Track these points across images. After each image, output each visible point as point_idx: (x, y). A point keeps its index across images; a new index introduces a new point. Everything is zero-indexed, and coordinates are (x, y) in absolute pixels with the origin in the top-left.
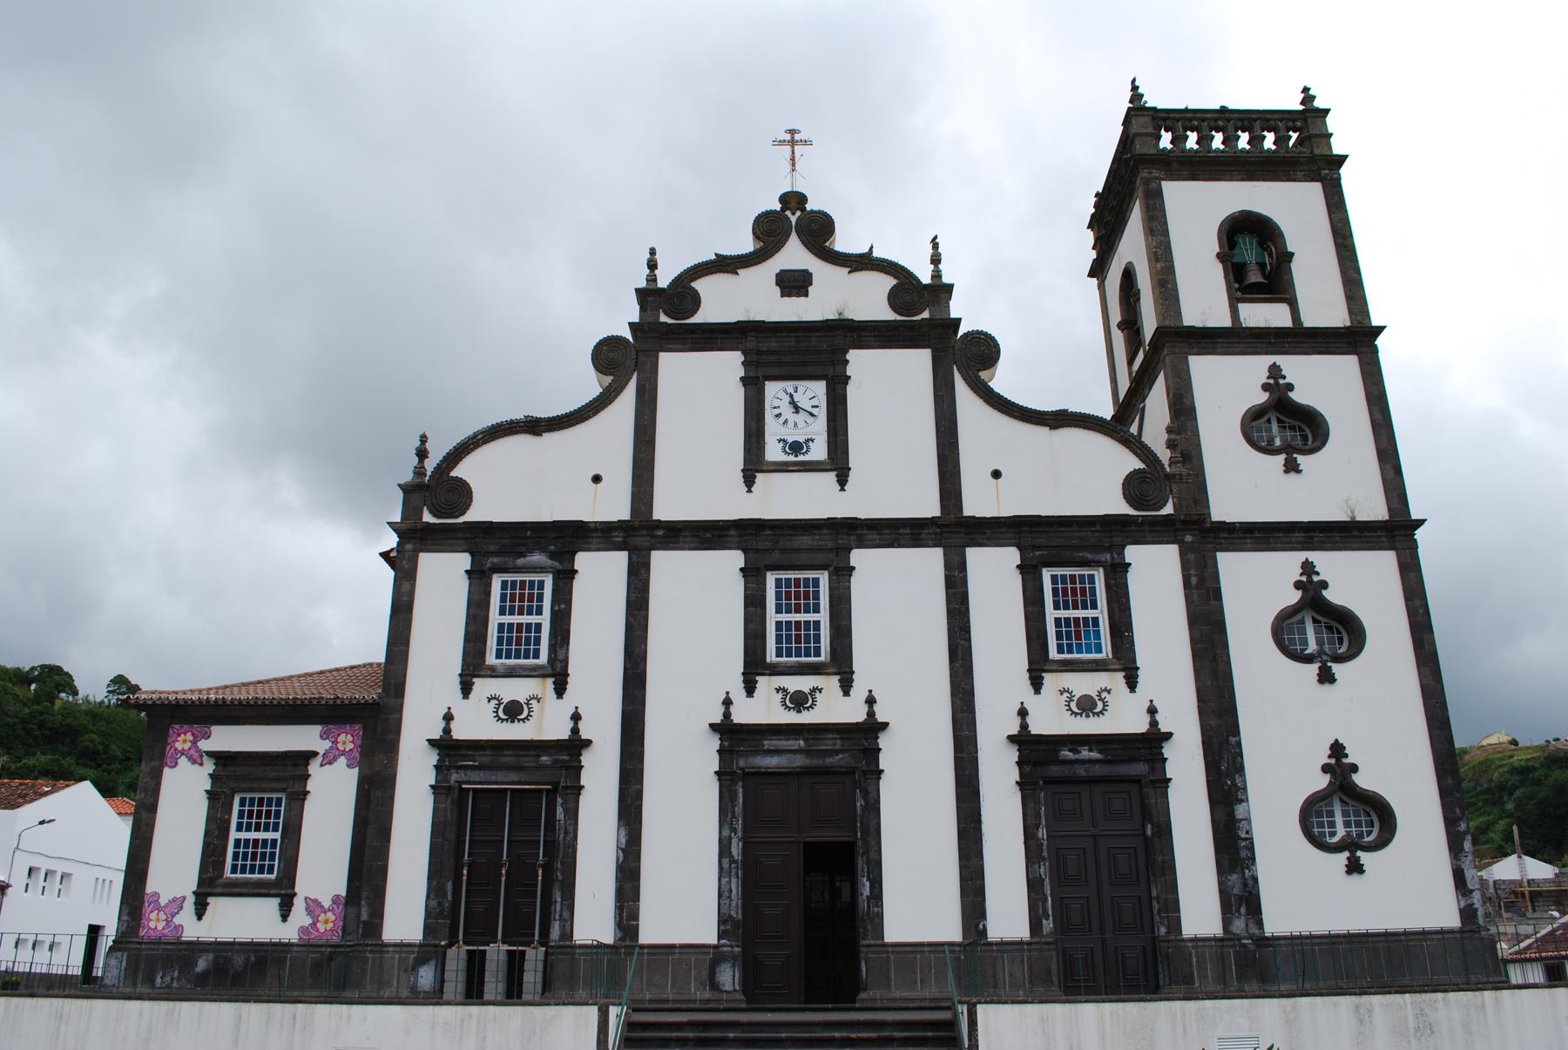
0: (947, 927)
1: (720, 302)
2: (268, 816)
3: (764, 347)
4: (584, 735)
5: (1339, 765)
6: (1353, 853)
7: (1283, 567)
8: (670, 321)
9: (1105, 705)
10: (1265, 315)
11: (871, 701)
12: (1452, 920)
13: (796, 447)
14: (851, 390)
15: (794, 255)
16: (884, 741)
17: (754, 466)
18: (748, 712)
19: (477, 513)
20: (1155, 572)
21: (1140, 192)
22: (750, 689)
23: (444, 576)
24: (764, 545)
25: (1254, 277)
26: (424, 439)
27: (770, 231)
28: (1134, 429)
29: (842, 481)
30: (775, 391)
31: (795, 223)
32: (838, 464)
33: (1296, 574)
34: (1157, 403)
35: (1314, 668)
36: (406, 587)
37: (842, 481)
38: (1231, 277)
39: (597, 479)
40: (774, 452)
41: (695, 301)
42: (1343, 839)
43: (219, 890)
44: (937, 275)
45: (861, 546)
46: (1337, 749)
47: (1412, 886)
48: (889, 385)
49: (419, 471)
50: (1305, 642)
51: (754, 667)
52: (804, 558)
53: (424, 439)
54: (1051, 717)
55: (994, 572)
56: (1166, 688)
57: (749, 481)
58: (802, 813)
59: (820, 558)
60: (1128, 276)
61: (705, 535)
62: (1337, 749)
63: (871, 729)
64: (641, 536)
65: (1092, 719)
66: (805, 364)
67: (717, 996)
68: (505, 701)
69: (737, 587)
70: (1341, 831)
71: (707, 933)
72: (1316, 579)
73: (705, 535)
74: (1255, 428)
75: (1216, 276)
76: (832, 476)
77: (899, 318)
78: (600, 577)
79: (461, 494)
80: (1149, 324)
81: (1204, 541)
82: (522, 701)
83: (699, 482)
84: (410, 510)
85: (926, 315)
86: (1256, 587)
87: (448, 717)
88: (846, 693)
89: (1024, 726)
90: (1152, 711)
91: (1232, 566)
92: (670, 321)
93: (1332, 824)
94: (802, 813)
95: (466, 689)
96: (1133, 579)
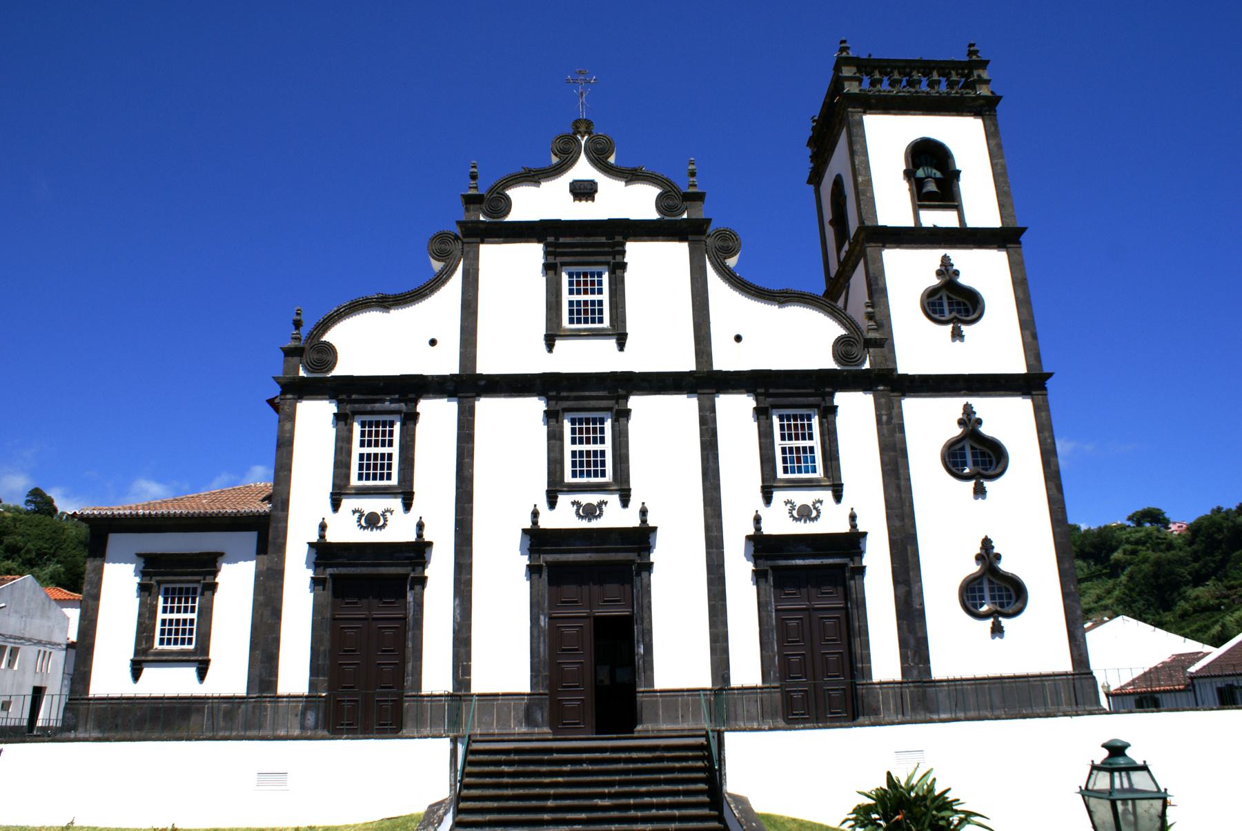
5: (987, 555)
10: (935, 218)
11: (644, 512)
22: (552, 504)
24: (563, 394)
29: (621, 346)
33: (959, 414)
36: (288, 426)
37: (621, 346)
41: (507, 204)
46: (987, 544)
54: (779, 523)
55: (736, 411)
56: (862, 502)
57: (550, 346)
62: (987, 544)
68: (366, 513)
78: (437, 416)
79: (328, 354)
81: (892, 387)
82: (379, 513)
87: (323, 527)
90: (853, 517)
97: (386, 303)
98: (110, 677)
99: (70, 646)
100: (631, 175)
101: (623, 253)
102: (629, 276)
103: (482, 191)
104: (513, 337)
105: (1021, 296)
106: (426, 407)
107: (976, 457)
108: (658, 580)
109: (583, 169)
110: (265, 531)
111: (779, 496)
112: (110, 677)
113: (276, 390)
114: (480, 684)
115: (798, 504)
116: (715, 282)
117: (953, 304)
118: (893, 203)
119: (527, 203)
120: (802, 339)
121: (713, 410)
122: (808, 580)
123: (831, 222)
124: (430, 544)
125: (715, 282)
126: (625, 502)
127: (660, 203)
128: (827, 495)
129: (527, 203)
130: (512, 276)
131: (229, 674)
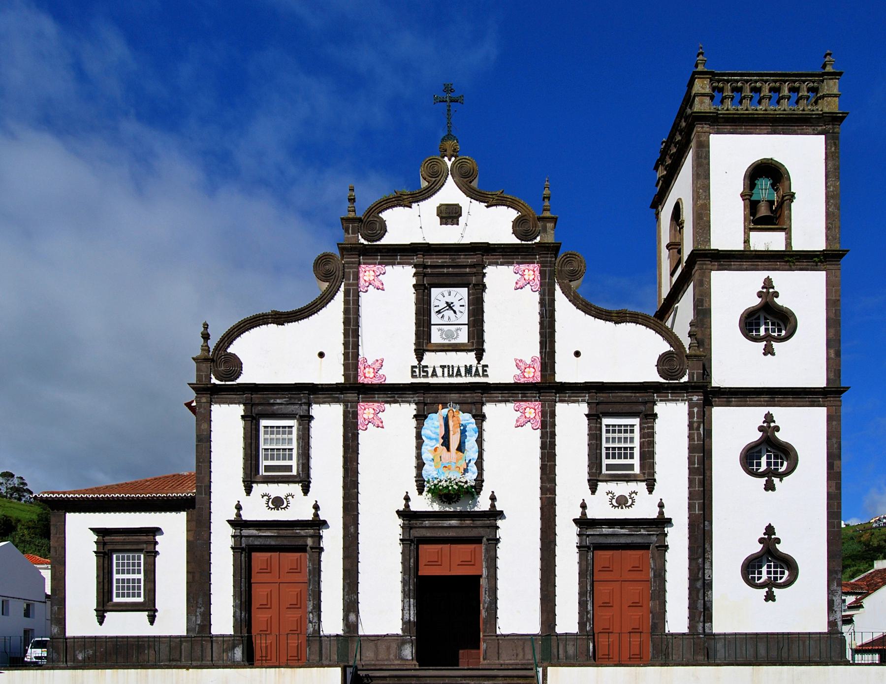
0: (533, 626)
2: (134, 565)
3: (429, 262)
4: (322, 517)
5: (769, 538)
7: (755, 415)
8: (366, 243)
9: (633, 501)
10: (768, 241)
11: (493, 498)
12: (825, 629)
20: (672, 418)
21: (693, 144)
24: (425, 396)
25: (763, 211)
26: (206, 326)
28: (668, 324)
30: (439, 297)
33: (760, 421)
34: (685, 306)
36: (204, 426)
38: (748, 210)
39: (321, 355)
40: (436, 337)
41: (383, 229)
42: (765, 582)
43: (110, 608)
45: (561, 401)
46: (770, 530)
47: (802, 607)
49: (206, 348)
50: (759, 464)
53: (206, 326)
54: (600, 507)
55: (572, 418)
58: (450, 542)
60: (677, 209)
61: (394, 393)
62: (770, 530)
65: (625, 510)
67: (403, 662)
68: (272, 497)
70: (765, 576)
71: (396, 628)
72: (772, 425)
73: (394, 393)
74: (750, 323)
75: (738, 208)
77: (519, 242)
78: (327, 418)
79: (235, 366)
80: (687, 249)
81: (707, 396)
82: (283, 497)
85: (538, 239)
86: (733, 428)
89: (584, 514)
90: (661, 506)
91: (720, 415)
92: (366, 243)
93: (760, 573)
94: (450, 542)
95: (593, 489)
96: (658, 425)
97: (281, 318)
98: (81, 620)
99: (211, 395)
100: (488, 197)
101: (484, 275)
103: (359, 215)
104: (390, 352)
105: (832, 316)
107: (769, 457)
109: (450, 192)
110: (196, 507)
111: (602, 487)
112: (81, 620)
113: (192, 395)
114: (367, 628)
116: (561, 301)
117: (768, 321)
118: (728, 229)
119: (406, 225)
120: (628, 353)
121: (553, 415)
122: (620, 551)
125: (561, 301)
127: (518, 227)
128: (642, 487)
129: (406, 225)
130: (389, 296)
131: (172, 620)
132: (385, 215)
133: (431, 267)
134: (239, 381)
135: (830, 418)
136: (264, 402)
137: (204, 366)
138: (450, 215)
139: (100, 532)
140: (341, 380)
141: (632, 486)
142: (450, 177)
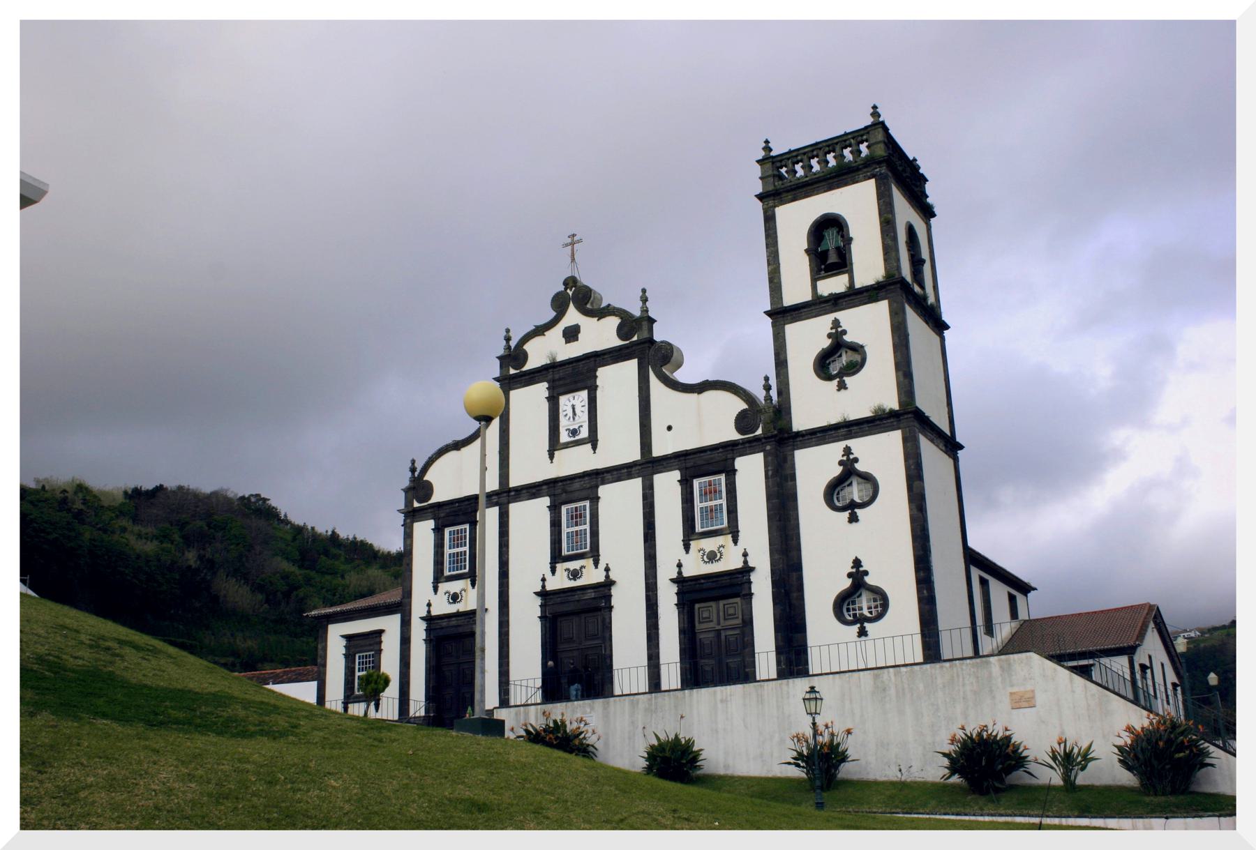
1: (539, 353)
4: (751, 564)
5: (858, 575)
6: (862, 624)
10: (834, 285)
11: (607, 570)
13: (574, 432)
14: (599, 392)
15: (573, 316)
16: (614, 591)
17: (555, 444)
18: (554, 584)
19: (438, 497)
20: (751, 471)
22: (553, 571)
23: (424, 530)
24: (560, 491)
27: (560, 305)
29: (594, 448)
30: (565, 402)
31: (577, 295)
32: (593, 440)
33: (839, 456)
35: (846, 514)
37: (594, 448)
40: (564, 437)
44: (645, 310)
45: (603, 483)
46: (857, 563)
48: (618, 382)
51: (557, 557)
52: (576, 495)
54: (695, 566)
55: (668, 484)
56: (753, 544)
57: (551, 456)
59: (584, 493)
61: (531, 491)
62: (857, 563)
63: (609, 584)
64: (505, 496)
66: (576, 382)
69: (546, 517)
73: (531, 491)
74: (822, 365)
76: (589, 446)
78: (491, 516)
83: (531, 464)
84: (408, 503)
86: (815, 468)
87: (680, 565)
88: (596, 567)
89: (680, 573)
95: (687, 548)
97: (457, 446)
102: (599, 393)
106: (741, 463)
108: (616, 616)
110: (402, 607)
111: (694, 545)
115: (707, 551)
116: (654, 380)
123: (924, 261)
124: (752, 569)
125: (654, 380)
126: (596, 564)
132: (525, 347)
133: (560, 379)
134: (431, 502)
135: (905, 440)
136: (462, 512)
137: (410, 494)
138: (572, 334)
139: (349, 638)
140: (638, 457)
141: (719, 540)
142: (571, 305)
